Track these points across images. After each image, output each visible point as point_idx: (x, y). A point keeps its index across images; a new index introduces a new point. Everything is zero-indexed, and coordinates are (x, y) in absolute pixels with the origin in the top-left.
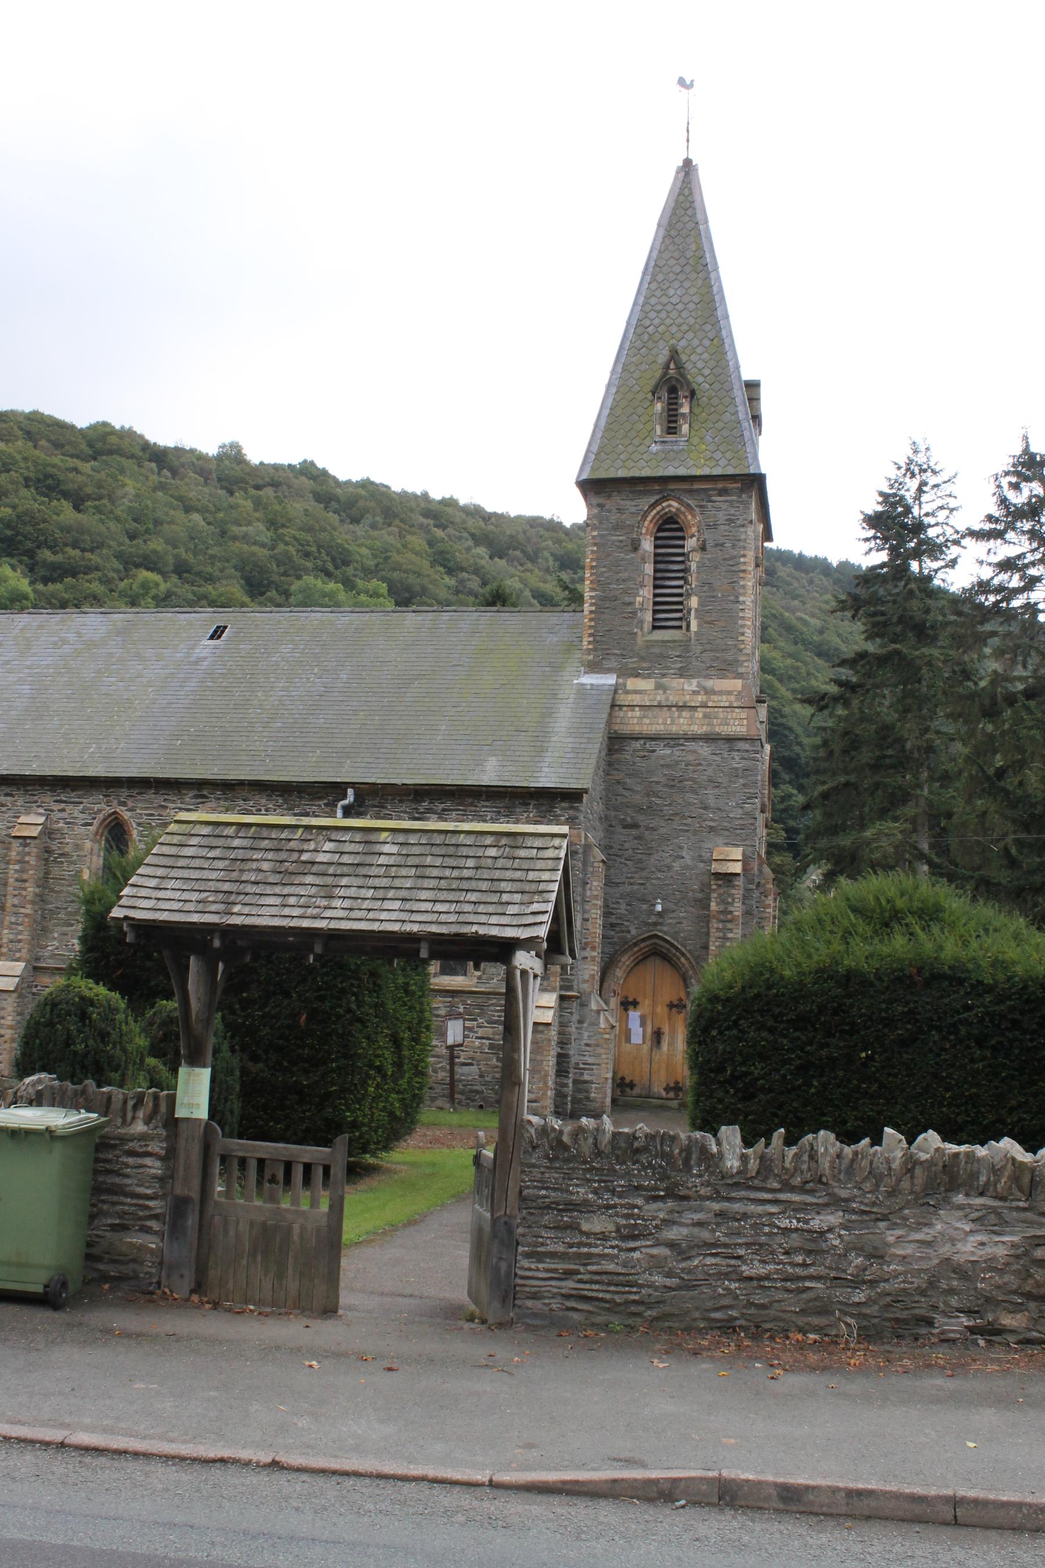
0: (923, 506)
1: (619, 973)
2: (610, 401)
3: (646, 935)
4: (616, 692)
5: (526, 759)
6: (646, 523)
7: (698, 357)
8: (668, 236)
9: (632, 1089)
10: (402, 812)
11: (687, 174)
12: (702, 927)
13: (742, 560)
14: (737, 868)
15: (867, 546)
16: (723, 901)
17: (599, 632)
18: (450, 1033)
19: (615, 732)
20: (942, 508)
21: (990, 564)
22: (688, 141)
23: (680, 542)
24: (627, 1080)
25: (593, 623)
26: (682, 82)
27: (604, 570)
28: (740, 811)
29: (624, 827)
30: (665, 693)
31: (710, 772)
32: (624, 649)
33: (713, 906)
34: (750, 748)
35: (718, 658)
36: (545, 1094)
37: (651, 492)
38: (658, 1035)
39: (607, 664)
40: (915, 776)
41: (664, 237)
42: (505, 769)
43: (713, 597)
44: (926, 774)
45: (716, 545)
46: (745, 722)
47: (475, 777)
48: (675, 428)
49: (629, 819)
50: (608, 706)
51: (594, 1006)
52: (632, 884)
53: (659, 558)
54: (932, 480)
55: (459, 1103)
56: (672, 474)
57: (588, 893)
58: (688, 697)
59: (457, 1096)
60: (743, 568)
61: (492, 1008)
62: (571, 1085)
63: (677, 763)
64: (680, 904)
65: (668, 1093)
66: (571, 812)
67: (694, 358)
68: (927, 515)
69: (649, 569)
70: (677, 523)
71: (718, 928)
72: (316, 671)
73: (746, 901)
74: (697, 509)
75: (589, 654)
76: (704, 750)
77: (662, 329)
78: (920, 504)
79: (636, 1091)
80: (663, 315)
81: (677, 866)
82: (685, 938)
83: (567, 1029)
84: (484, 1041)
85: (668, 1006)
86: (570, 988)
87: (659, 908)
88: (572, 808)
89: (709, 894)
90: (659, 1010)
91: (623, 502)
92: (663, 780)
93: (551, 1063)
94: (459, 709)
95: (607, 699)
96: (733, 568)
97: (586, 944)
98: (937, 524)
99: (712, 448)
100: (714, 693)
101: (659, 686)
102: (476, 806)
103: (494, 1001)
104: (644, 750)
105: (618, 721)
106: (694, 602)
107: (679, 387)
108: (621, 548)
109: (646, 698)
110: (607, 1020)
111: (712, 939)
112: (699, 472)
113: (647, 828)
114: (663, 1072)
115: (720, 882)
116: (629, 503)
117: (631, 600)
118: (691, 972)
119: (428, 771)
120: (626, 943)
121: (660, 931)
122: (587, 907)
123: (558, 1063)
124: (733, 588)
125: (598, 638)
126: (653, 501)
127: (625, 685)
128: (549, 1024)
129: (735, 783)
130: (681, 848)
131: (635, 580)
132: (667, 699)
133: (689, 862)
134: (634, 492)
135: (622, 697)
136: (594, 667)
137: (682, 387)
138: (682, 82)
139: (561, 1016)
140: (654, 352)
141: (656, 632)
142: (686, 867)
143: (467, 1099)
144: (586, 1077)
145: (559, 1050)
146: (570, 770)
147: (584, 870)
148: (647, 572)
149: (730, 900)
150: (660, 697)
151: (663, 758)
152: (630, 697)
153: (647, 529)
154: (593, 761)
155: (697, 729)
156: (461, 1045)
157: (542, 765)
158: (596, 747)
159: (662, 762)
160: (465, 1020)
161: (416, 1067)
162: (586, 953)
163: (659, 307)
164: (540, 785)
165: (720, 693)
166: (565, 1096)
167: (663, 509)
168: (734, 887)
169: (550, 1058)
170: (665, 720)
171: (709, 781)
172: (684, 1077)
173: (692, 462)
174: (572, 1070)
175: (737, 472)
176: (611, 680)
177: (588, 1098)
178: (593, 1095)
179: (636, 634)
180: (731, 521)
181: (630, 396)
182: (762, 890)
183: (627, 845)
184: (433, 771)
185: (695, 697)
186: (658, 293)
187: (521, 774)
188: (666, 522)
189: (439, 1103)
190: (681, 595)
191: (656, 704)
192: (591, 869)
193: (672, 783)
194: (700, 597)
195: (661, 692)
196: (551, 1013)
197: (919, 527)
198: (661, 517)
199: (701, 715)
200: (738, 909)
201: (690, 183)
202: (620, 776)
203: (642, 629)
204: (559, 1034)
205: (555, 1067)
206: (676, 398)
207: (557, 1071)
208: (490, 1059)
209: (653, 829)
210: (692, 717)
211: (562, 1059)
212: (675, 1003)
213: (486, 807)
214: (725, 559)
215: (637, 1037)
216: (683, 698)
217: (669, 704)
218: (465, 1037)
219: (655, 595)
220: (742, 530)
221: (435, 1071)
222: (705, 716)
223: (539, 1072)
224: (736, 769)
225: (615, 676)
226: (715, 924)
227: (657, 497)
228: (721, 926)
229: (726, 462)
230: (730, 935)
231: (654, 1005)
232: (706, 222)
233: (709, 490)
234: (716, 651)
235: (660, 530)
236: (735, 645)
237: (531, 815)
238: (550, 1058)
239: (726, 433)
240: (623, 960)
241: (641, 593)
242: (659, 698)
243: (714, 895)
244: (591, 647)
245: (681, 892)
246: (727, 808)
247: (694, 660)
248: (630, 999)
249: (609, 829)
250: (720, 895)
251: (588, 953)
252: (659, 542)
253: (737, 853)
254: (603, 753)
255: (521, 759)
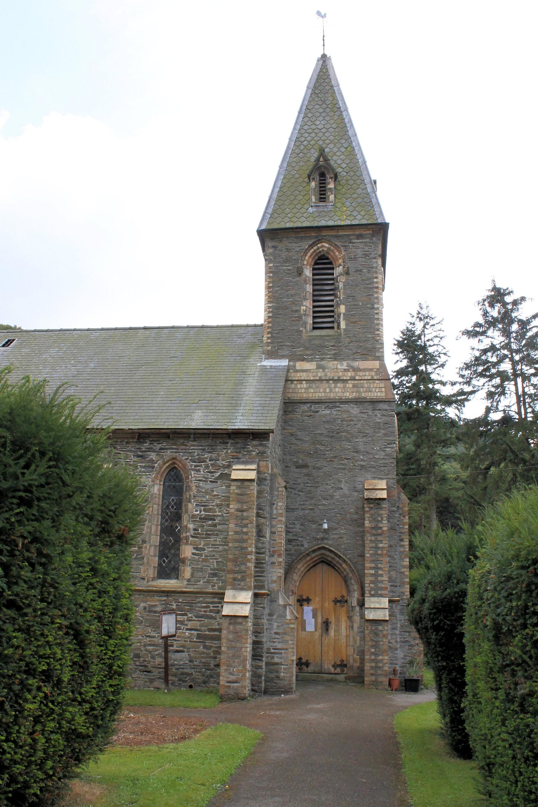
0: (426, 336)
1: (296, 577)
2: (279, 184)
3: (316, 547)
4: (288, 371)
5: (224, 411)
6: (307, 258)
7: (338, 158)
8: (313, 93)
9: (307, 667)
10: (128, 451)
11: (324, 61)
12: (358, 540)
13: (375, 280)
14: (384, 495)
15: (397, 357)
16: (374, 519)
17: (275, 330)
18: (164, 625)
19: (289, 399)
20: (436, 337)
21: (478, 350)
22: (324, 45)
23: (331, 271)
24: (304, 660)
25: (270, 325)
26: (319, 13)
27: (278, 289)
28: (383, 453)
29: (297, 467)
30: (324, 371)
31: (359, 426)
32: (293, 342)
33: (367, 523)
34: (388, 408)
35: (361, 346)
36: (244, 675)
37: (310, 238)
38: (326, 624)
39: (281, 353)
40: (428, 478)
41: (311, 94)
42: (209, 418)
43: (355, 305)
44: (433, 478)
45: (356, 271)
46: (383, 390)
47: (186, 423)
48: (325, 198)
49: (300, 461)
50: (284, 381)
51: (281, 602)
52: (304, 509)
53: (316, 282)
54: (432, 322)
55: (173, 684)
56: (324, 225)
57: (275, 512)
58: (341, 374)
59: (170, 678)
60: (376, 285)
61: (199, 605)
62: (264, 667)
63: (335, 420)
64: (341, 524)
65: (335, 669)
66: (260, 448)
67: (334, 158)
68: (428, 341)
69: (309, 288)
70: (328, 259)
71: (371, 540)
72: (72, 363)
73: (391, 520)
74: (342, 248)
75: (268, 346)
76: (355, 410)
77: (312, 142)
78: (425, 335)
79: (311, 668)
80: (313, 135)
81: (337, 495)
82: (345, 549)
83: (260, 621)
84: (193, 632)
85: (333, 601)
86: (262, 587)
87: (325, 526)
88: (261, 445)
89: (364, 515)
90: (326, 605)
91: (290, 245)
92: (325, 432)
93: (248, 649)
94: (174, 382)
95: (283, 374)
96: (369, 286)
97: (274, 552)
98: (434, 345)
99: (351, 209)
100: (360, 370)
101: (319, 367)
102: (186, 445)
103: (201, 599)
104: (311, 411)
105: (291, 391)
106: (342, 309)
107: (326, 172)
108: (290, 274)
109: (311, 374)
110: (292, 613)
111: (367, 549)
112: (343, 223)
113: (314, 468)
114: (331, 653)
115: (371, 506)
116: (294, 245)
117: (297, 308)
118: (351, 575)
119: (150, 421)
120: (301, 554)
121: (326, 544)
122: (274, 523)
123: (254, 649)
124: (370, 299)
125: (274, 335)
126: (311, 243)
127: (295, 366)
128: (247, 617)
129: (378, 433)
130: (340, 482)
131: (300, 295)
132: (326, 375)
133: (347, 492)
134: (297, 238)
135: (293, 374)
136: (271, 355)
137: (328, 173)
138: (319, 13)
139: (255, 610)
140: (308, 155)
141: (315, 331)
142: (344, 496)
143: (180, 680)
144: (276, 660)
145: (254, 638)
146: (258, 418)
147: (271, 494)
148: (308, 290)
149: (379, 519)
150: (320, 374)
151: (324, 416)
152: (298, 374)
153: (308, 262)
154: (275, 417)
155: (348, 395)
156: (174, 636)
157: (237, 414)
158: (277, 404)
159: (324, 420)
160: (177, 615)
161: (110, 666)
162: (274, 559)
163: (310, 131)
164: (237, 427)
165: (364, 370)
166: (260, 676)
167: (318, 248)
168: (381, 508)
169: (248, 645)
170: (325, 389)
171: (360, 432)
172: (347, 656)
173: (338, 218)
174: (265, 655)
175: (369, 222)
176: (284, 363)
177: (278, 677)
178: (282, 674)
179: (301, 331)
180: (367, 255)
181: (293, 180)
182: (401, 512)
183: (299, 481)
184: (153, 421)
185: (346, 373)
186: (309, 123)
187: (221, 421)
188: (320, 258)
189: (156, 684)
190: (332, 306)
191: (318, 378)
192: (276, 493)
193: (331, 434)
194: (346, 306)
195: (321, 370)
196: (248, 607)
197: (423, 348)
198: (317, 254)
199: (351, 386)
200: (385, 525)
201: (326, 66)
202: (293, 430)
203: (305, 328)
204: (254, 625)
205: (251, 653)
206: (325, 180)
207: (253, 656)
208: (198, 647)
209: (319, 468)
210: (344, 387)
211: (257, 644)
212: (339, 599)
213: (194, 446)
214: (363, 280)
215: (310, 626)
216: (337, 374)
217: (327, 378)
218: (177, 628)
219: (314, 307)
220: (374, 261)
221: (153, 657)
222: (354, 386)
223: (239, 657)
224: (379, 423)
225: (287, 360)
226: (368, 538)
227: (313, 241)
228: (373, 538)
229: (361, 217)
230: (381, 545)
231: (323, 601)
232: (338, 85)
233: (349, 235)
234: (359, 341)
235: (316, 264)
236: (373, 338)
237: (229, 451)
238: (248, 645)
239: (359, 200)
240: (299, 567)
241: (304, 304)
242: (319, 374)
243: (367, 515)
244: (269, 341)
245: (341, 514)
246: (374, 451)
247: (343, 348)
248: (305, 597)
249: (286, 468)
250: (372, 515)
251: (275, 559)
252: (316, 272)
253: (383, 484)
254: (281, 413)
255: (220, 411)
